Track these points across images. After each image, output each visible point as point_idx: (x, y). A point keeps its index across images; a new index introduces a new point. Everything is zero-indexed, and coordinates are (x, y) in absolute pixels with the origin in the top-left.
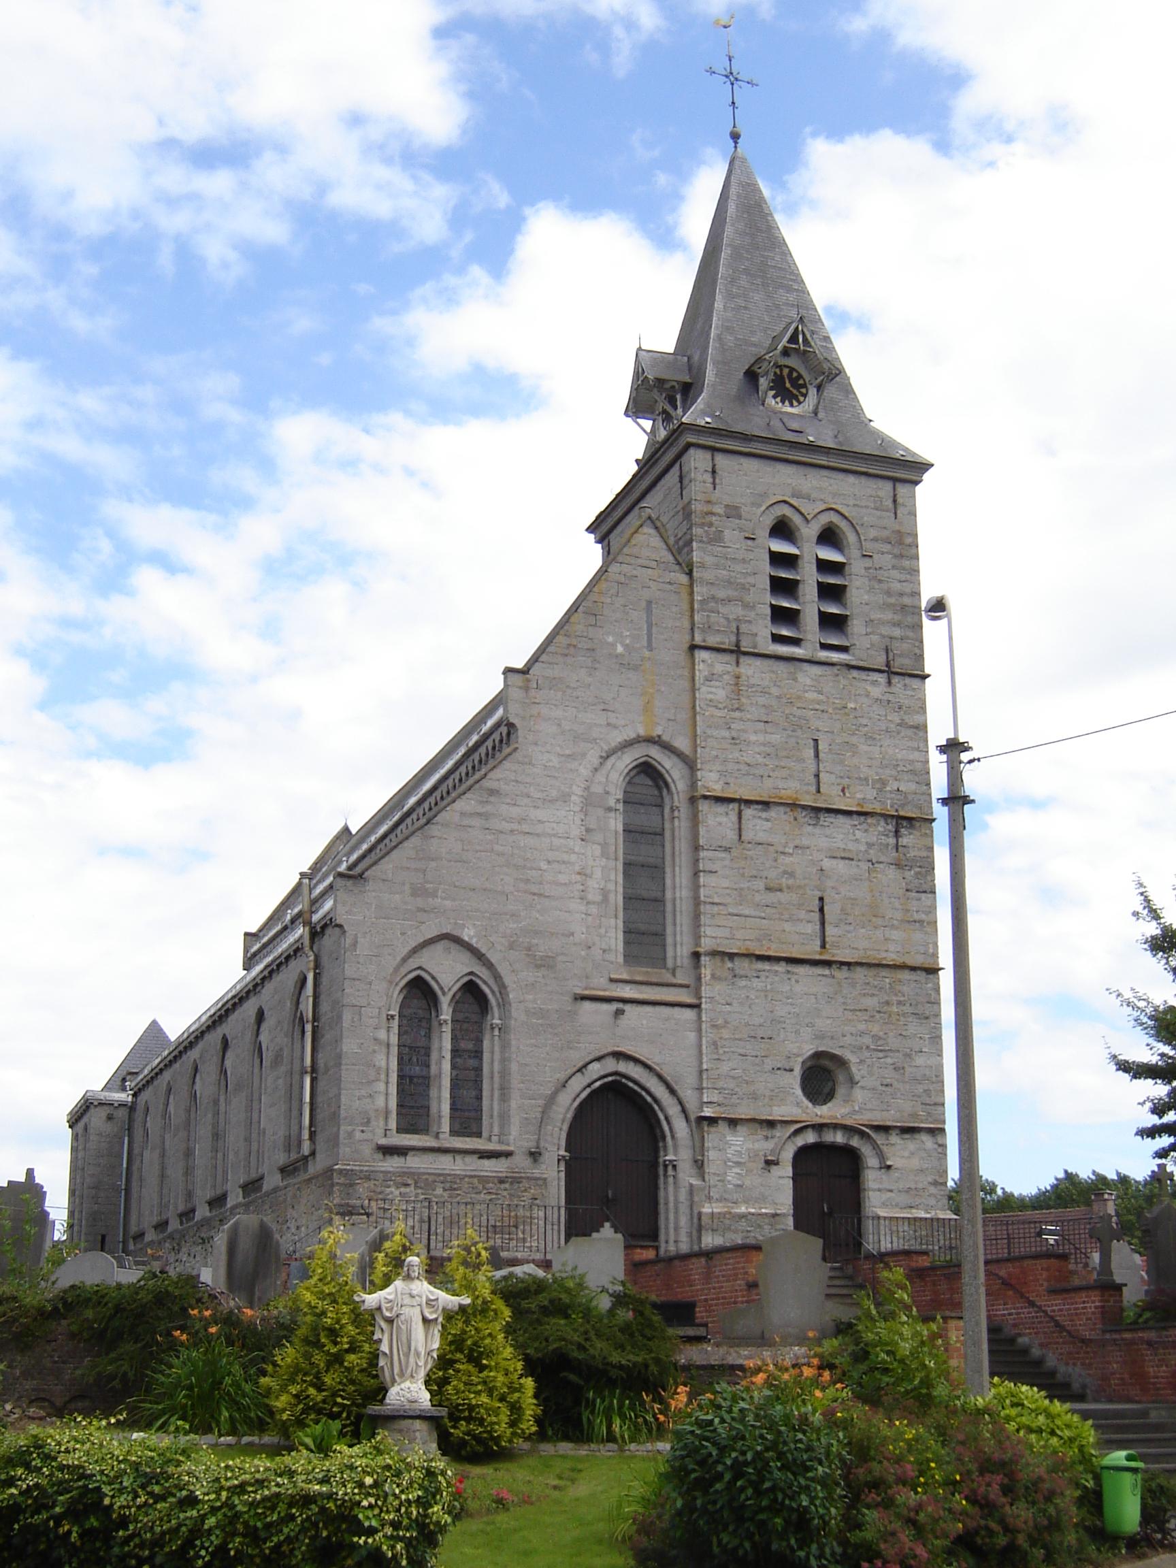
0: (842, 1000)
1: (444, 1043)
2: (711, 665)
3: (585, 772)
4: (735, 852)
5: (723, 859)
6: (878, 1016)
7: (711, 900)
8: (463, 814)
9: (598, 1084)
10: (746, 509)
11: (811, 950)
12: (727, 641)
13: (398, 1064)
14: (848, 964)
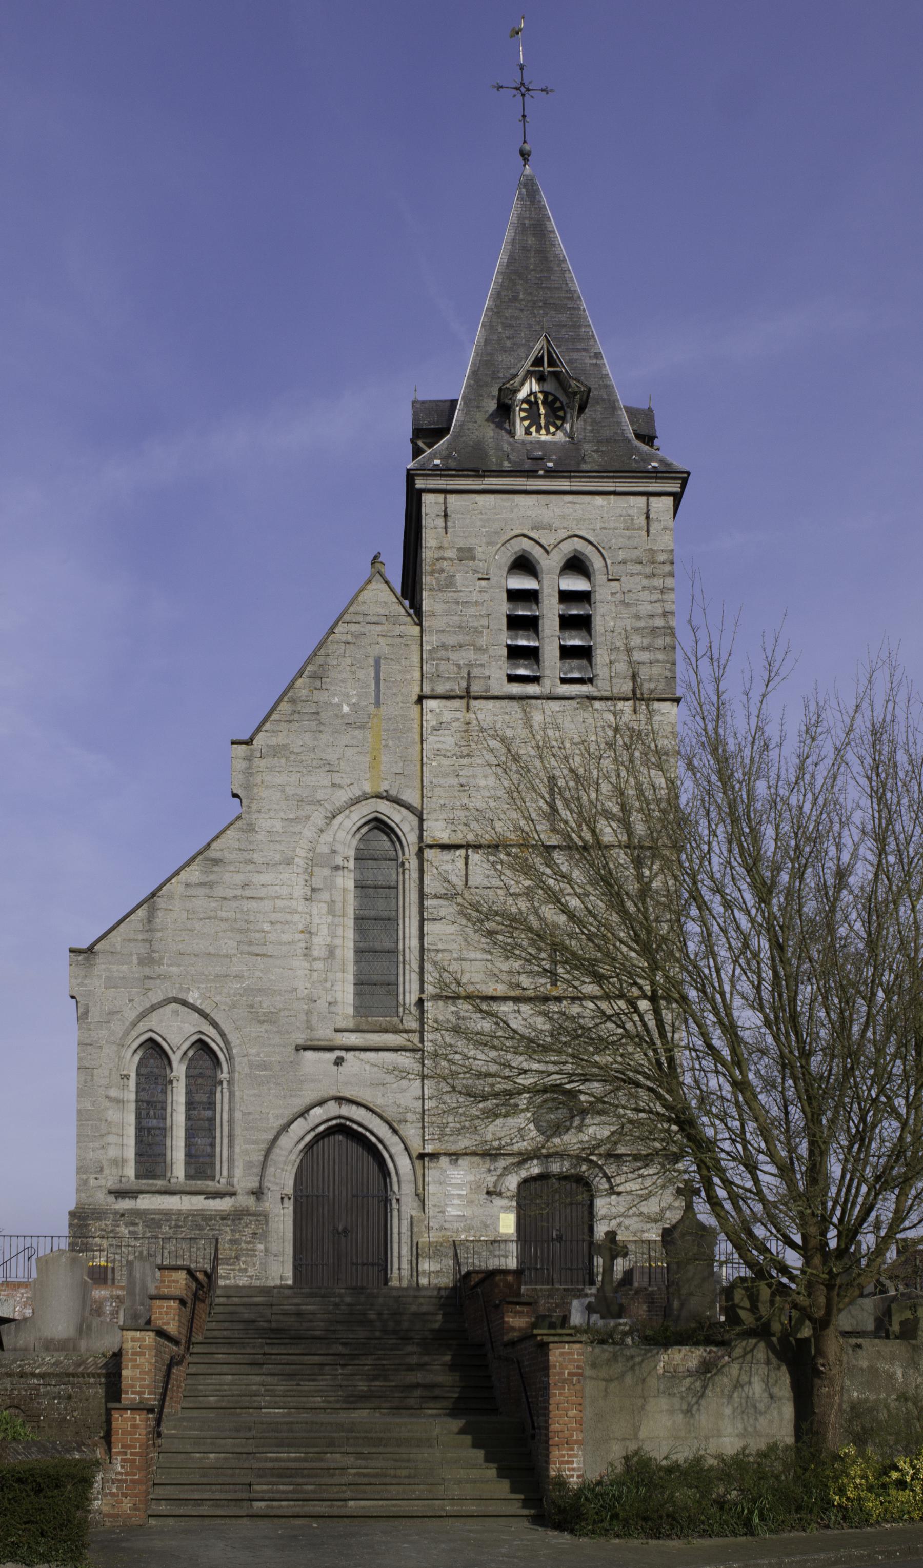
1: (178, 1096)
2: (440, 714)
3: (308, 832)
7: (435, 947)
9: (322, 1128)
10: (480, 549)
13: (136, 1118)
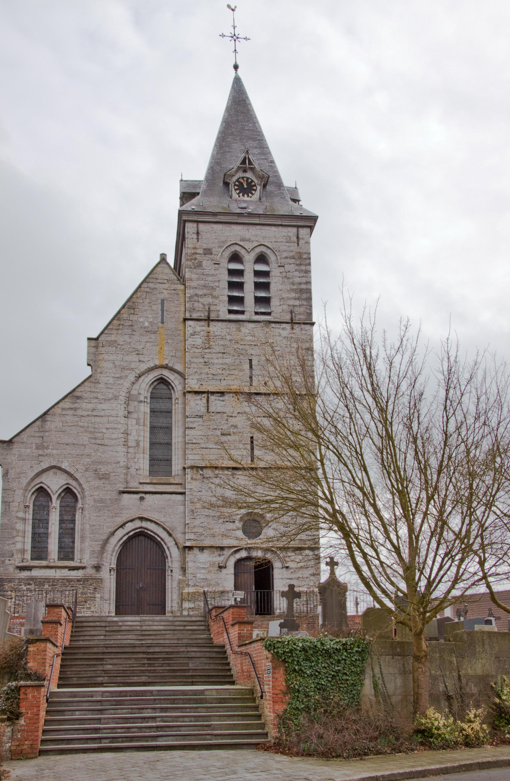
1: (54, 518)
3: (127, 384)
4: (204, 418)
5: (198, 422)
8: (63, 409)
10: (215, 250)
12: (203, 315)
13: (32, 528)
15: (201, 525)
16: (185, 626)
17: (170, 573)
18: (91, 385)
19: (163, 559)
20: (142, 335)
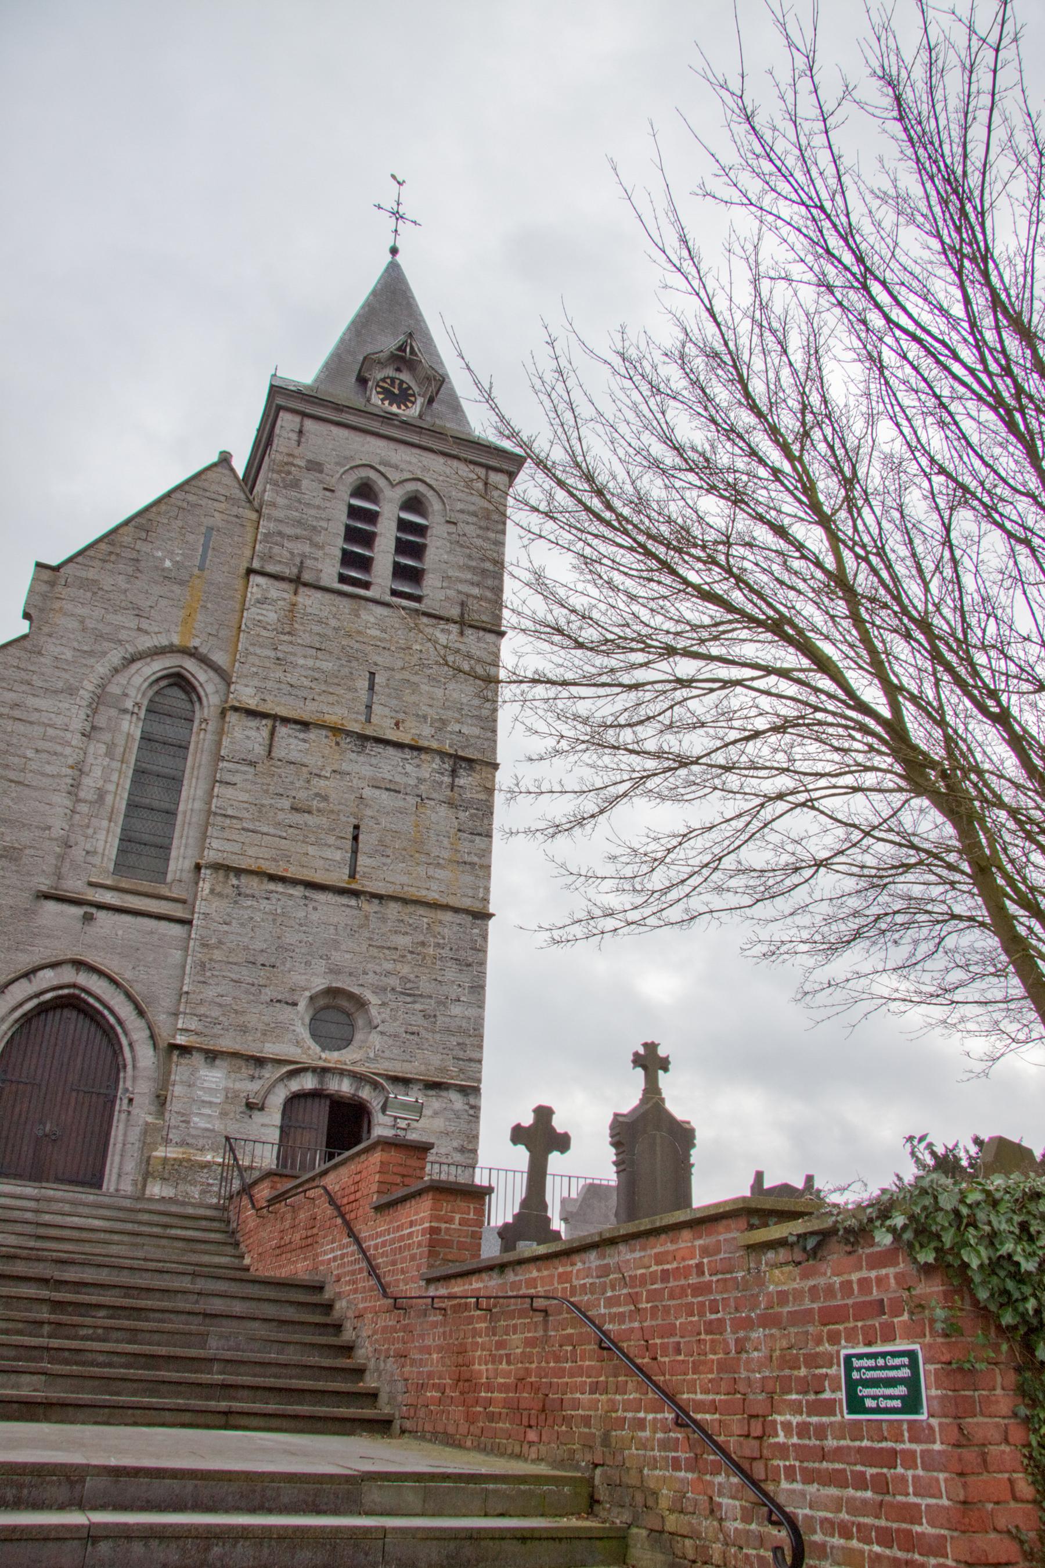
0: (367, 935)
2: (267, 590)
4: (260, 768)
5: (245, 773)
6: (409, 956)
9: (49, 996)
11: (339, 877)
14: (380, 897)
15: (218, 1000)
16: (166, 1226)
17: (125, 1107)
18: (22, 654)
19: (114, 1072)
20: (156, 582)
